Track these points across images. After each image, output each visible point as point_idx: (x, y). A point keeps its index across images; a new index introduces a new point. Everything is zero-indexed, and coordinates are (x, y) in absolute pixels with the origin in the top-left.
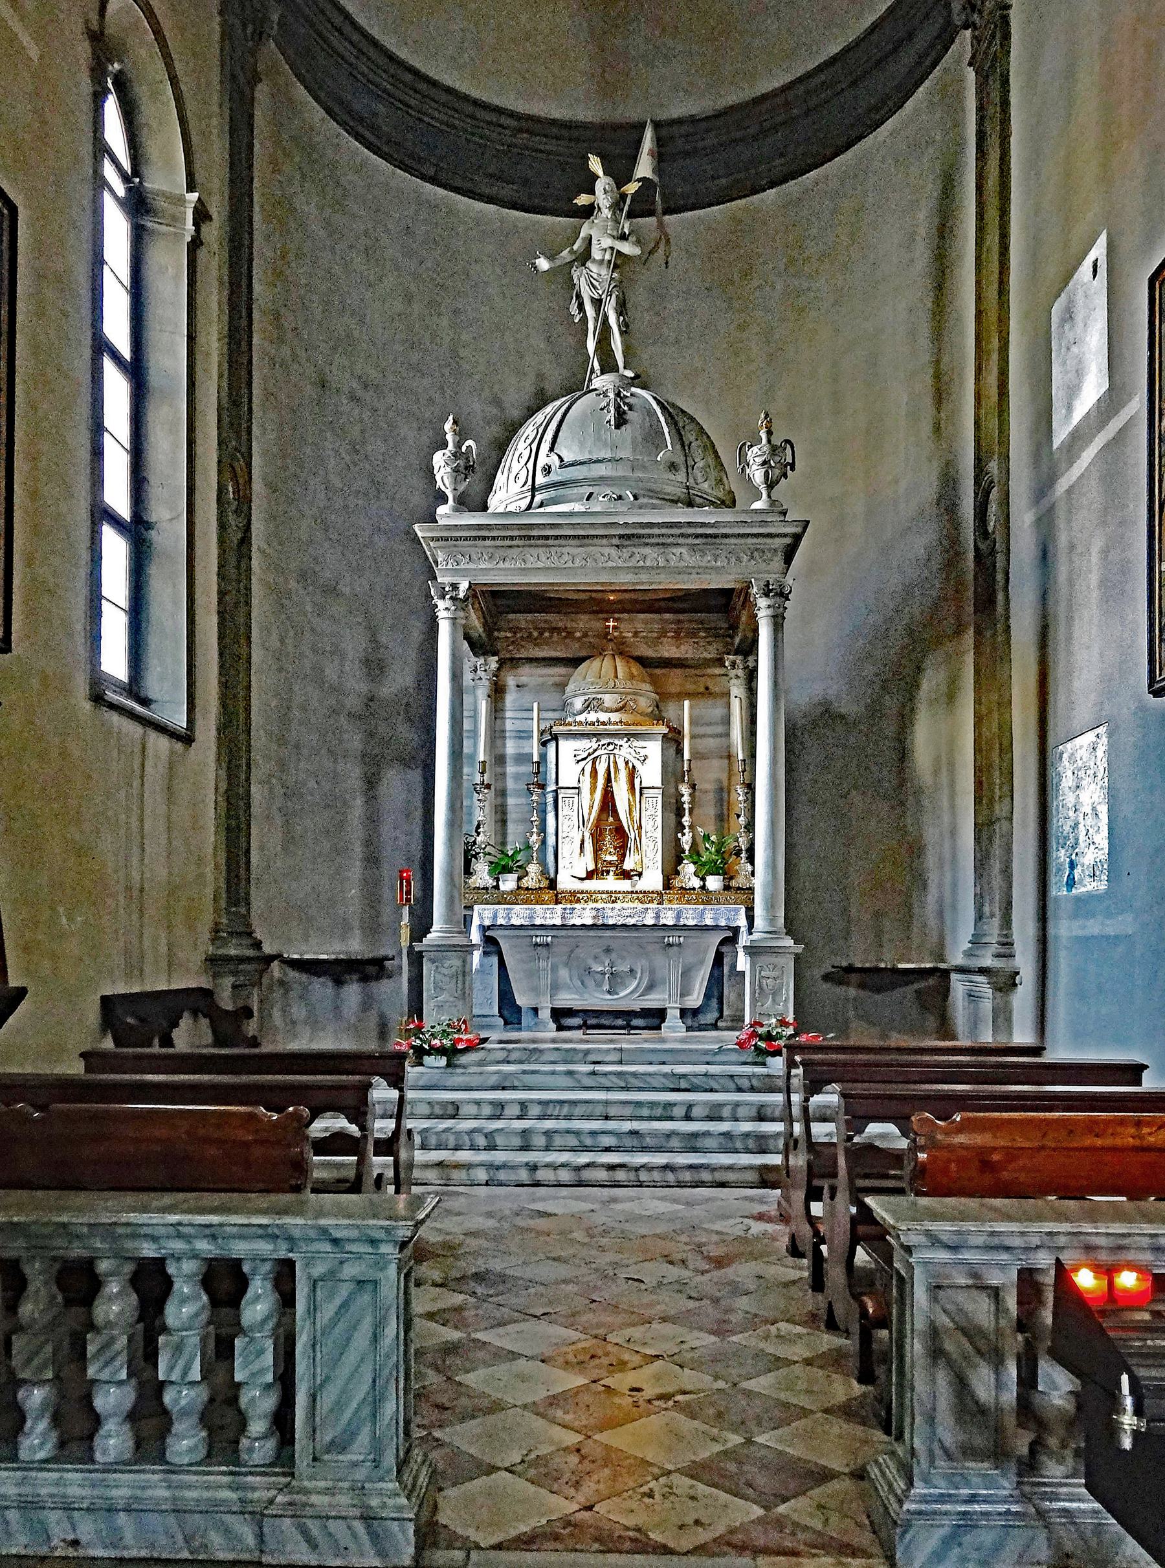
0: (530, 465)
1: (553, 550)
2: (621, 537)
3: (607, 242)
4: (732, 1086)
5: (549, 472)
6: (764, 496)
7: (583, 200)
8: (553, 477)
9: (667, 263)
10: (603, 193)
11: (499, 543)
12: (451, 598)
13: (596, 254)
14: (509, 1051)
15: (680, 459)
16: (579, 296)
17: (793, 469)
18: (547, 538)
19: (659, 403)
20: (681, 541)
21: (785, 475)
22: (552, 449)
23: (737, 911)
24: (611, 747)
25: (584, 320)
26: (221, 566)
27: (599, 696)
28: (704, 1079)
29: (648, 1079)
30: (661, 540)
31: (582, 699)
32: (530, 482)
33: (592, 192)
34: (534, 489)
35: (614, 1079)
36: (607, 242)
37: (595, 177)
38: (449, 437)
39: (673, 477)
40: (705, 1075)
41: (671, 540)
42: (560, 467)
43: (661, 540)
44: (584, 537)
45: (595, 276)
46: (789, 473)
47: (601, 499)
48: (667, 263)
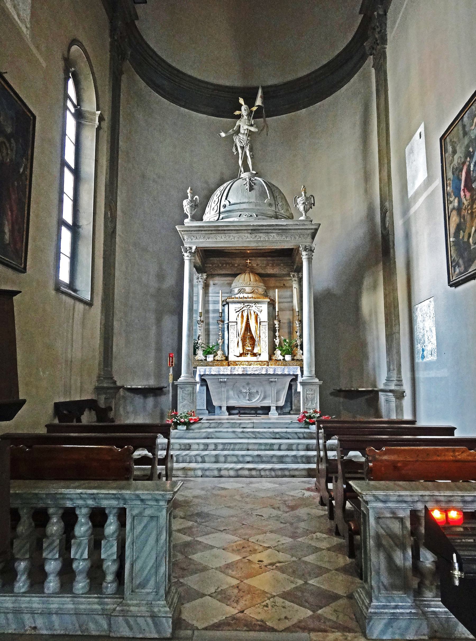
1: (227, 235)
2: (252, 230)
3: (246, 127)
7: (237, 113)
8: (227, 209)
13: (242, 131)
14: (210, 423)
15: (273, 202)
17: (314, 205)
18: (225, 230)
20: (274, 231)
21: (311, 208)
28: (286, 434)
29: (264, 434)
30: (266, 231)
36: (246, 127)
38: (189, 195)
39: (270, 209)
41: (270, 231)
43: (266, 231)
44: (238, 230)
46: (313, 207)
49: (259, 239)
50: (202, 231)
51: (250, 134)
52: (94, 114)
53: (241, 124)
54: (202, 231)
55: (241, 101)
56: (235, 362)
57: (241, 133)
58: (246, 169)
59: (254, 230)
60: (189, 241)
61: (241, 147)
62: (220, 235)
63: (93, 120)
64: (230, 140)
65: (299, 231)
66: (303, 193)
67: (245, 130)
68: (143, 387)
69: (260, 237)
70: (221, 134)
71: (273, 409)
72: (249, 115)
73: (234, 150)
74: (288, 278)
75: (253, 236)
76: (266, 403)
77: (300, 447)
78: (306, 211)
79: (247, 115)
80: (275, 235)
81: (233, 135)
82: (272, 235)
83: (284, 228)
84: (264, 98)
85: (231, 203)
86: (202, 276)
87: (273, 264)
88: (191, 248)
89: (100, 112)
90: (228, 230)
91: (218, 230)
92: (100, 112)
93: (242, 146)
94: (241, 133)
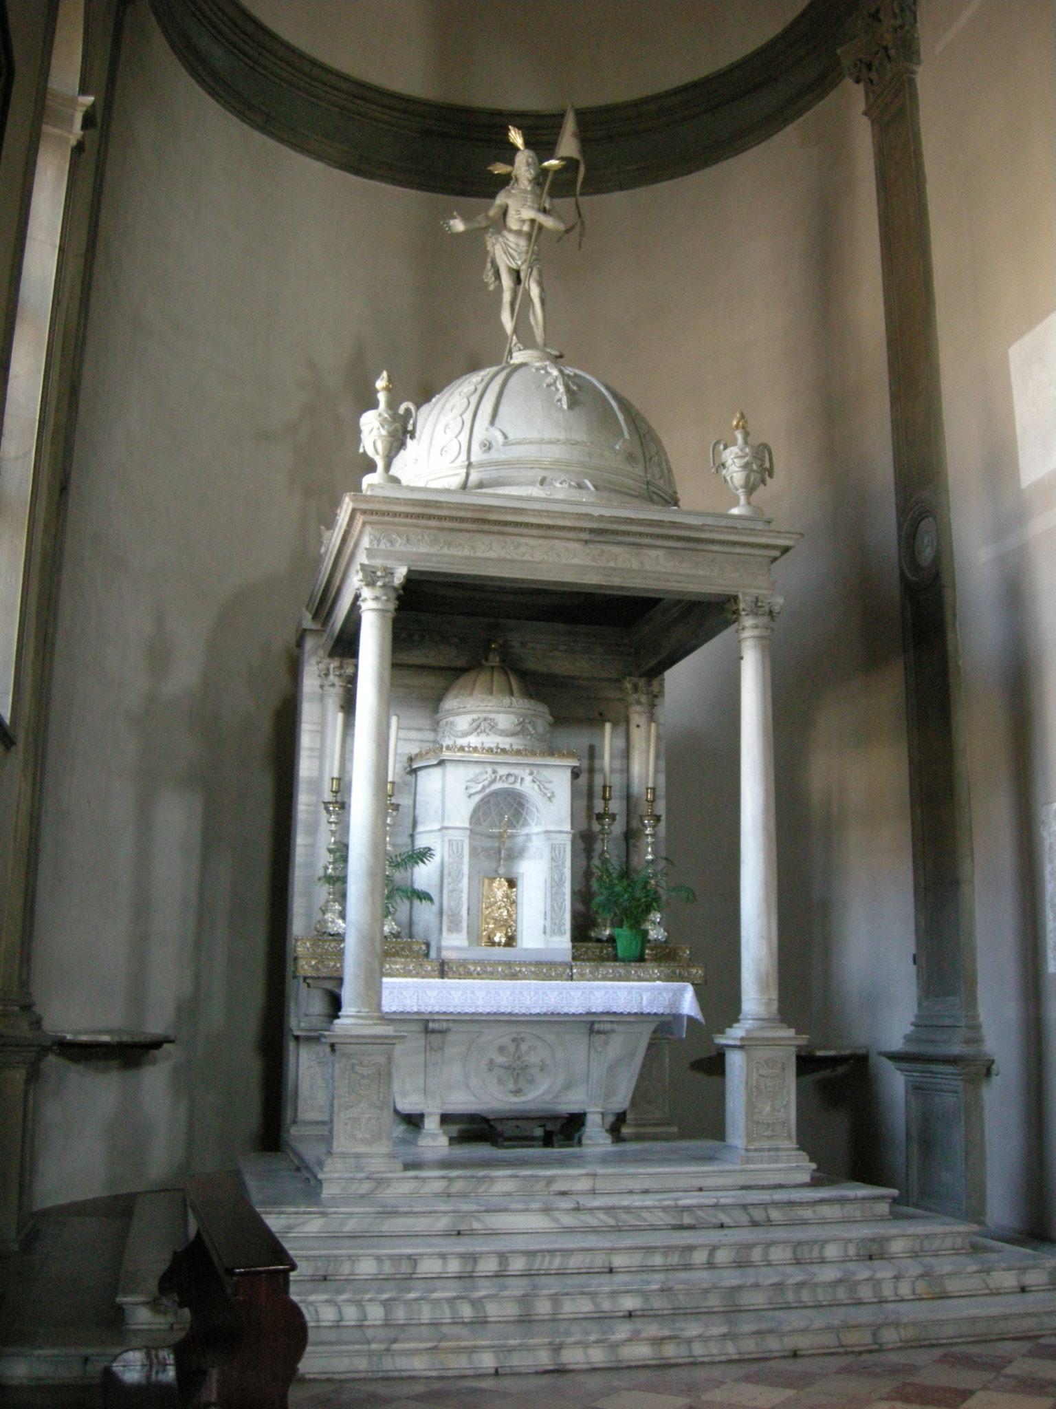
0: (464, 438)
1: (508, 539)
2: (592, 531)
3: (528, 214)
4: (744, 1219)
5: (490, 448)
6: (743, 500)
7: (499, 169)
8: (494, 455)
9: (580, 244)
10: (523, 166)
11: (446, 524)
12: (384, 586)
13: (513, 223)
14: (450, 1179)
15: (638, 451)
16: (493, 262)
17: (771, 475)
18: (506, 523)
19: (607, 388)
20: (659, 542)
21: (763, 482)
22: (492, 423)
23: (682, 991)
24: (511, 779)
25: (499, 289)
26: (647, 520)
27: (492, 716)
28: (712, 1211)
29: (645, 1214)
30: (638, 540)
31: (469, 718)
32: (463, 456)
33: (511, 162)
34: (470, 465)
35: (602, 1216)
36: (528, 214)
37: (515, 149)
38: (382, 397)
39: (630, 469)
40: (715, 1206)
41: (647, 541)
42: (505, 444)
43: (638, 540)
44: (549, 527)
45: (513, 245)
46: (768, 479)
47: (558, 485)
48: (580, 244)
49: (612, 564)
50: (429, 517)
51: (536, 232)
52: (73, 102)
53: (510, 202)
54: (429, 517)
55: (516, 137)
56: (463, 963)
57: (510, 231)
58: (527, 341)
59: (601, 532)
60: (382, 546)
61: (510, 270)
62: (486, 539)
63: (68, 122)
64: (474, 245)
65: (737, 550)
66: (739, 436)
67: (523, 221)
68: (116, 1039)
69: (616, 558)
70: (452, 222)
71: (432, 1124)
72: (540, 178)
73: (489, 277)
74: (613, 694)
75: (593, 549)
76: (570, 1103)
77: (722, 1256)
78: (750, 489)
79: (530, 181)
80: (660, 553)
81: (486, 229)
82: (653, 553)
83: (694, 534)
84: (585, 139)
85: (511, 437)
86: (341, 667)
87: (422, 637)
88: (389, 573)
89: (91, 99)
90: (517, 524)
91: (485, 521)
92: (91, 99)
93: (514, 266)
94: (510, 231)
